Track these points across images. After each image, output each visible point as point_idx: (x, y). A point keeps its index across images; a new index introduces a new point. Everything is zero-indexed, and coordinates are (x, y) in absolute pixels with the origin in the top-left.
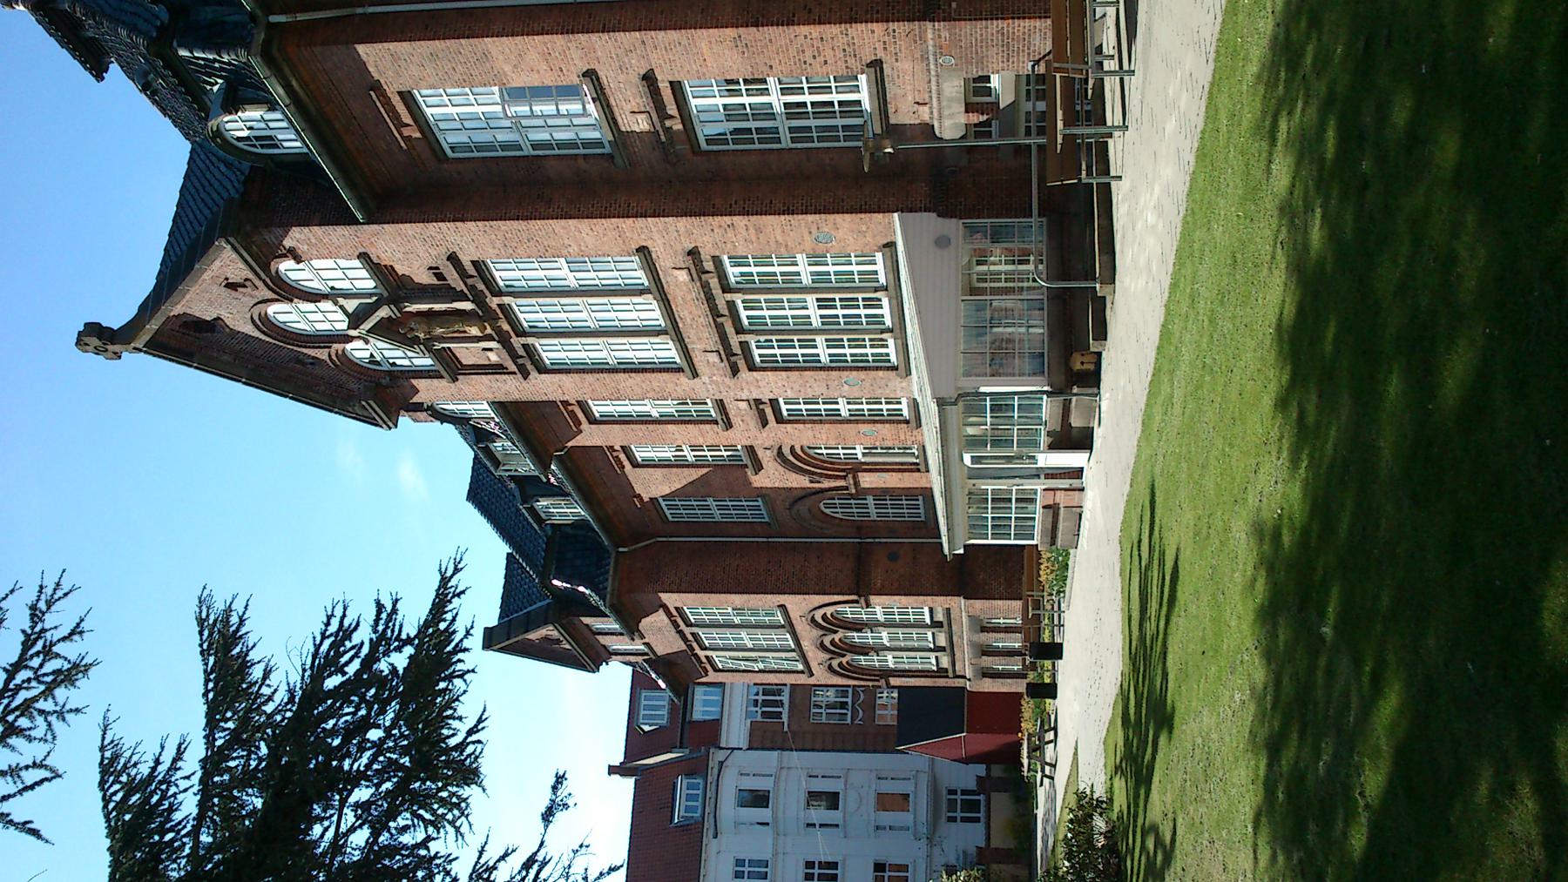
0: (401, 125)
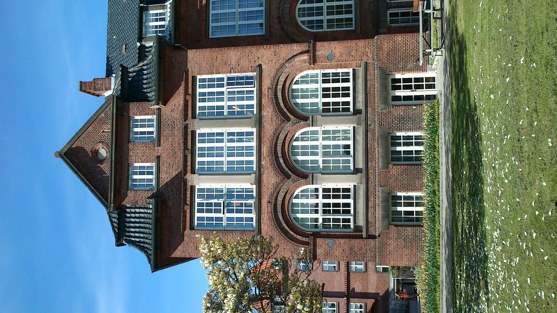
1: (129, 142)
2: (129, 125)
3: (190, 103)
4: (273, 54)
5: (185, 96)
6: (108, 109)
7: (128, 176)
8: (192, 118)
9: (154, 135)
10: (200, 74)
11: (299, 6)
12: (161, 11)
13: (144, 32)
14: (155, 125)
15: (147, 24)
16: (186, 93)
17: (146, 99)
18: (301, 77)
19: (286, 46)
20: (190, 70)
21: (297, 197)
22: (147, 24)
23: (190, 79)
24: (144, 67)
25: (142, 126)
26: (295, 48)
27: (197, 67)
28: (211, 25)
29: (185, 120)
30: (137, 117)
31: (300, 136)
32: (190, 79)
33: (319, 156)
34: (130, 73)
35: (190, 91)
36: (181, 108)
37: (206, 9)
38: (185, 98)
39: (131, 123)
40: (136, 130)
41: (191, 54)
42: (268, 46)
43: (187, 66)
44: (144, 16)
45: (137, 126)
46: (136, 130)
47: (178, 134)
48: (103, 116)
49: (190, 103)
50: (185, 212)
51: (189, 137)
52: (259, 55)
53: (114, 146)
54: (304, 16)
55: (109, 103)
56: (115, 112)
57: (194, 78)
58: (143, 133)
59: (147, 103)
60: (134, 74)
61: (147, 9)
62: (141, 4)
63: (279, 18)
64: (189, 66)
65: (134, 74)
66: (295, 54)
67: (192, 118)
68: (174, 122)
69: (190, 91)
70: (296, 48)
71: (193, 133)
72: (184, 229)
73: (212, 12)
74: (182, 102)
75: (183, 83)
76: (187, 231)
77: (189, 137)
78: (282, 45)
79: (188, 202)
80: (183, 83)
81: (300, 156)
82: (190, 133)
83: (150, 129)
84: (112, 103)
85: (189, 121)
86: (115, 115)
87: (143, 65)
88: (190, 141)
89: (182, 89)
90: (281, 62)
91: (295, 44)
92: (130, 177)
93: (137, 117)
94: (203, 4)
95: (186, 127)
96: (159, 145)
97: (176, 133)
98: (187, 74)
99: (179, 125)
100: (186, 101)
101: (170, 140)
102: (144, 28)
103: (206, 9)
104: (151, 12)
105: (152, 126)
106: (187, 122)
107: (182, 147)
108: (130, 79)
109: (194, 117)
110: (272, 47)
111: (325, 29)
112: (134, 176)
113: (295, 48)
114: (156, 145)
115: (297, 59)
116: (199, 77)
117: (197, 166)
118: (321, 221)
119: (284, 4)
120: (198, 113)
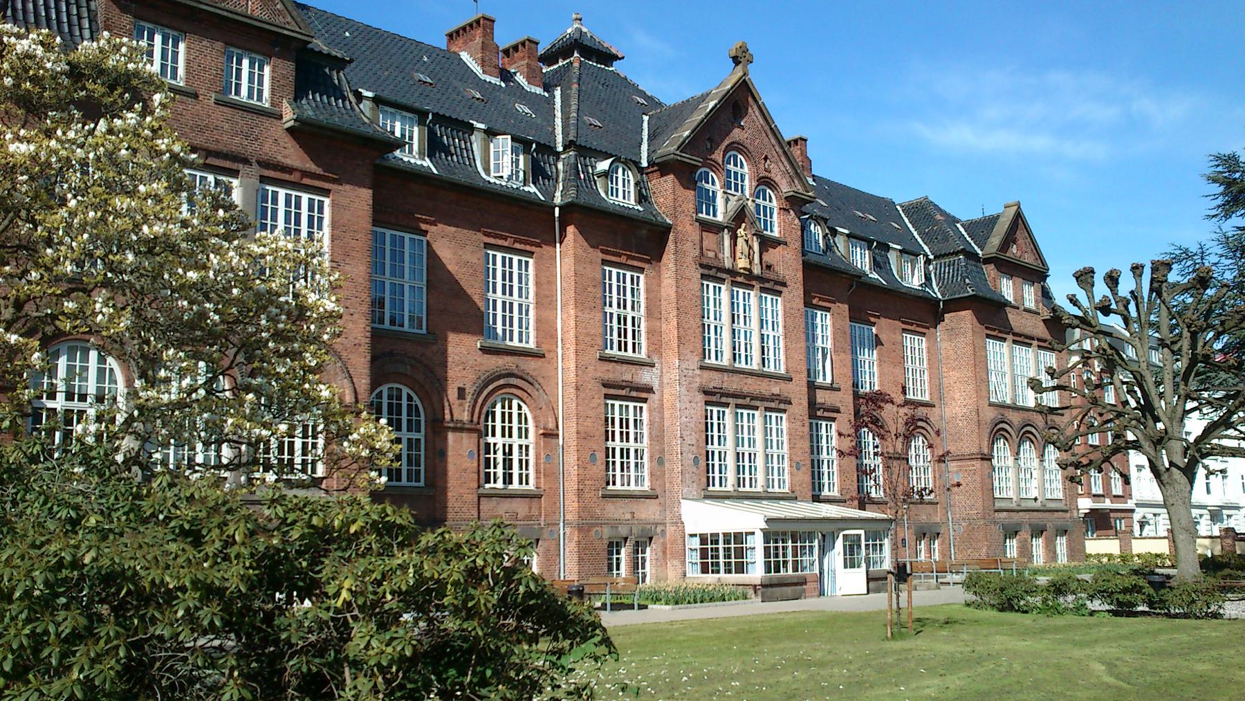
0: (820, 299)
1: (226, 44)
2: (257, 52)
3: (286, 177)
4: (356, 342)
5: (301, 171)
6: (289, 19)
7: (162, 25)
8: (261, 176)
9: (233, 96)
10: (334, 205)
11: (405, 391)
12: (416, 147)
13: (386, 108)
14: (251, 102)
15: (398, 117)
16: (305, 174)
17: (299, 95)
18: (111, 370)
19: (368, 365)
20: (340, 188)
21: (102, 360)
22: (398, 117)
23: (327, 186)
24: (347, 102)
25: (251, 75)
26: (363, 381)
27: (345, 202)
28: (388, 233)
29: (259, 163)
30: (267, 69)
31: (107, 366)
32: (327, 186)
33: (64, 403)
34: (338, 73)
35: (306, 181)
36: (279, 158)
37: (412, 228)
38: (296, 170)
39: (258, 57)
40: (246, 63)
41: (366, 194)
42: (368, 334)
43: (349, 182)
44: (411, 115)
45: (252, 65)
46: (246, 63)
47: (235, 144)
48: (278, 6)
49: (286, 177)
50: (619, 255)
51: (227, 164)
52: (356, 316)
53: (225, 14)
54: (390, 397)
55: (301, 25)
56: (286, 32)
57: (326, 193)
58: (239, 77)
59: (291, 96)
60: (336, 82)
61: (421, 123)
62: (433, 114)
63: (391, 354)
64: (348, 187)
65: (336, 82)
66: (355, 380)
67: (261, 176)
68: (256, 140)
69: (306, 181)
70: (363, 383)
71: (234, 173)
72: (603, 251)
73: (407, 236)
74: (288, 162)
75: (319, 171)
76: (601, 256)
77: (227, 164)
78: (369, 358)
79: (630, 262)
80: (319, 171)
81: (65, 363)
82: (235, 166)
83: (244, 91)
84: (298, 30)
85: (255, 170)
86: (280, 31)
87: (350, 103)
88: (222, 165)
89: (311, 166)
90: (344, 354)
91: (369, 381)
92: (159, 27)
93: (267, 69)
94: (421, 225)
95: (246, 161)
96: (218, 102)
97: (237, 140)
98: (334, 181)
99: (250, 149)
100: (289, 170)
101: (226, 126)
102: (392, 110)
103: (412, 228)
104: (416, 129)
105: (250, 96)
106: (255, 166)
107: (212, 146)
108: (327, 70)
109: (264, 180)
110: (368, 340)
111: (421, 436)
112: (160, 37)
113: (363, 381)
114: (221, 97)
115: (346, 382)
116: (327, 201)
117: (270, 188)
118: (50, 404)
119: (411, 365)
120: (267, 187)
